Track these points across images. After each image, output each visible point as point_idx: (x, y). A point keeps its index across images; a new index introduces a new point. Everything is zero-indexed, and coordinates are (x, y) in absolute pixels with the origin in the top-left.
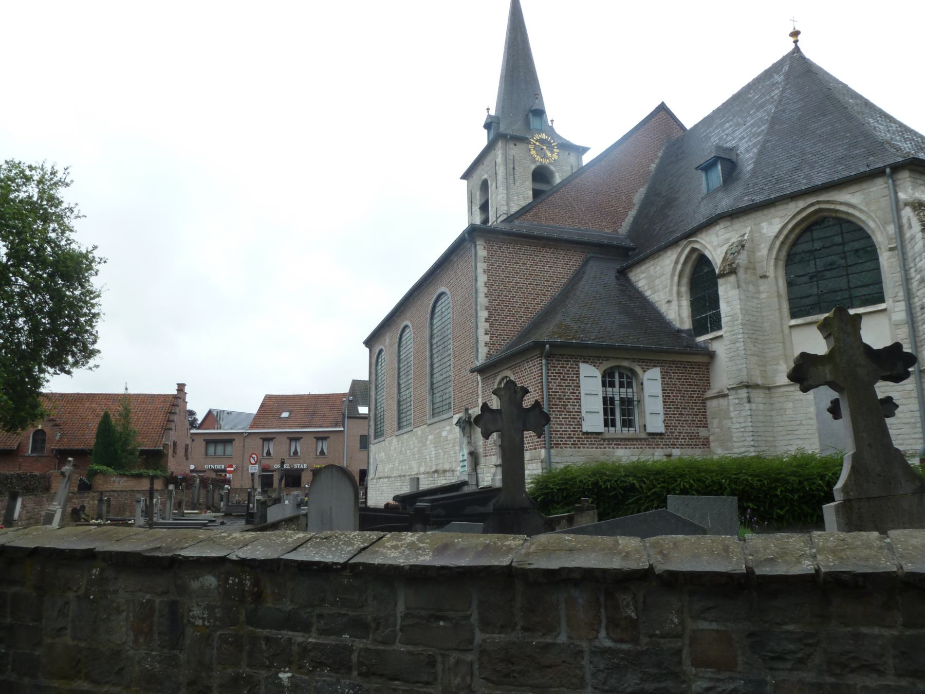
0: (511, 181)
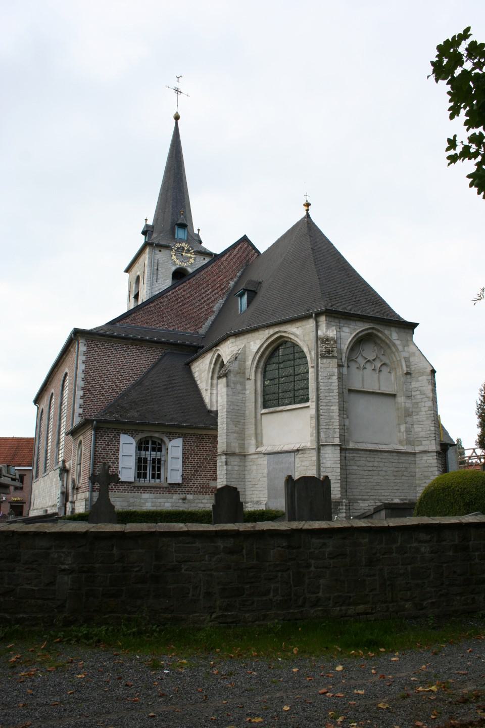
0: (155, 279)
